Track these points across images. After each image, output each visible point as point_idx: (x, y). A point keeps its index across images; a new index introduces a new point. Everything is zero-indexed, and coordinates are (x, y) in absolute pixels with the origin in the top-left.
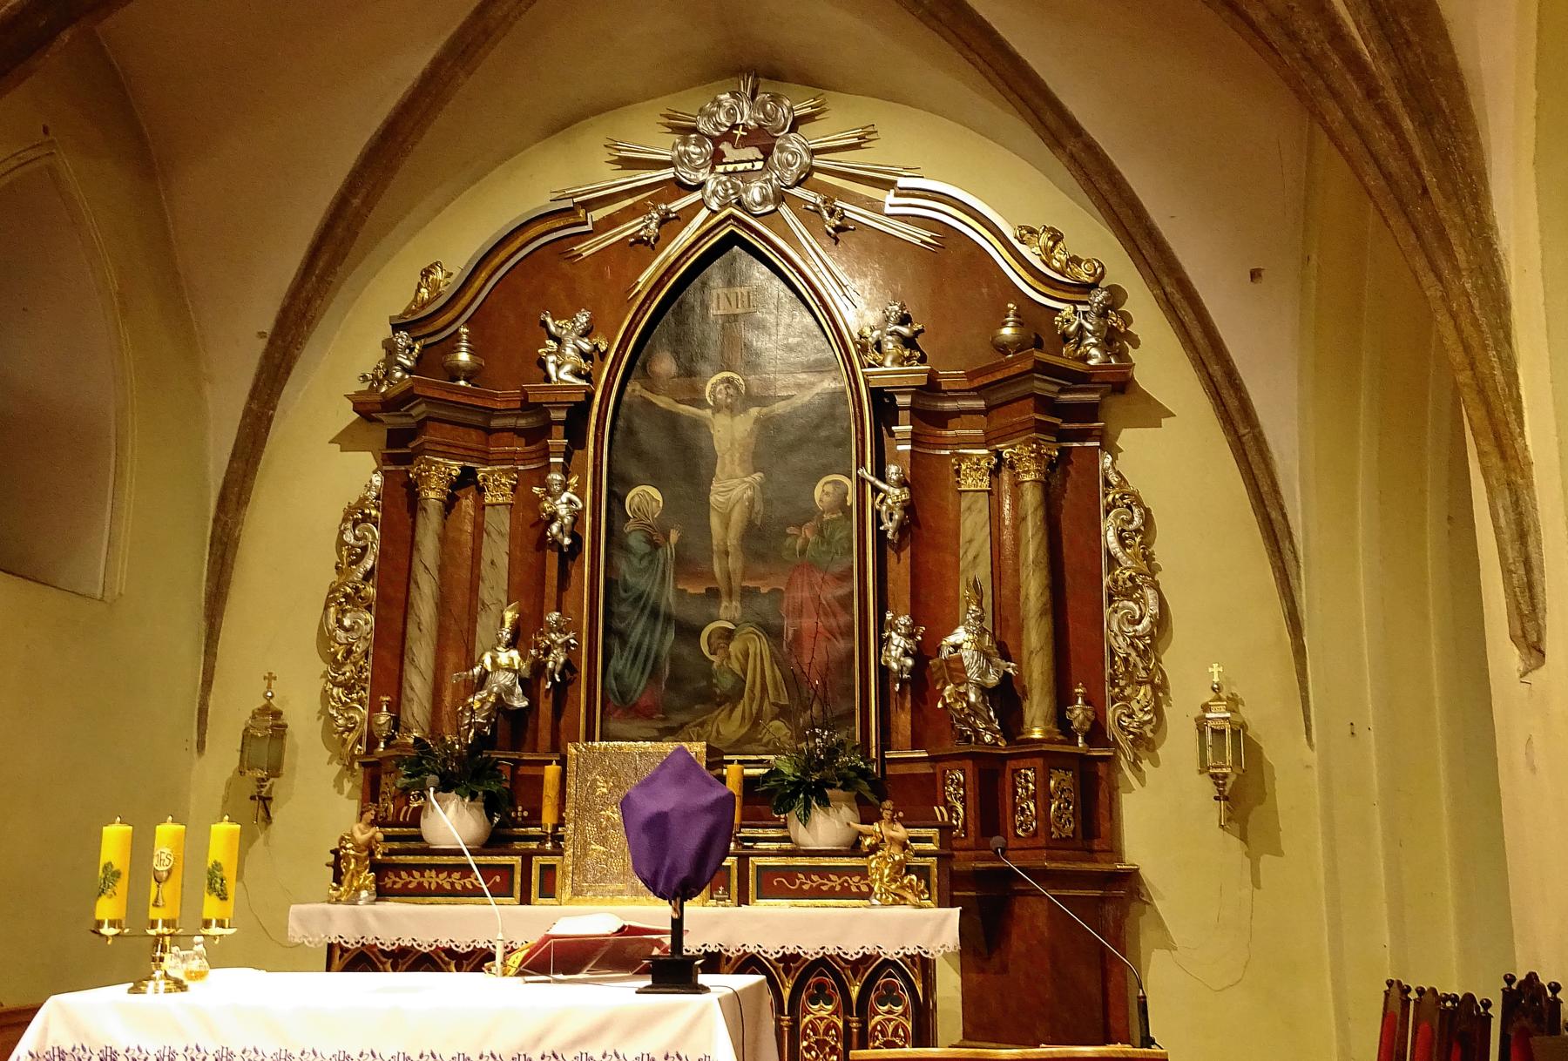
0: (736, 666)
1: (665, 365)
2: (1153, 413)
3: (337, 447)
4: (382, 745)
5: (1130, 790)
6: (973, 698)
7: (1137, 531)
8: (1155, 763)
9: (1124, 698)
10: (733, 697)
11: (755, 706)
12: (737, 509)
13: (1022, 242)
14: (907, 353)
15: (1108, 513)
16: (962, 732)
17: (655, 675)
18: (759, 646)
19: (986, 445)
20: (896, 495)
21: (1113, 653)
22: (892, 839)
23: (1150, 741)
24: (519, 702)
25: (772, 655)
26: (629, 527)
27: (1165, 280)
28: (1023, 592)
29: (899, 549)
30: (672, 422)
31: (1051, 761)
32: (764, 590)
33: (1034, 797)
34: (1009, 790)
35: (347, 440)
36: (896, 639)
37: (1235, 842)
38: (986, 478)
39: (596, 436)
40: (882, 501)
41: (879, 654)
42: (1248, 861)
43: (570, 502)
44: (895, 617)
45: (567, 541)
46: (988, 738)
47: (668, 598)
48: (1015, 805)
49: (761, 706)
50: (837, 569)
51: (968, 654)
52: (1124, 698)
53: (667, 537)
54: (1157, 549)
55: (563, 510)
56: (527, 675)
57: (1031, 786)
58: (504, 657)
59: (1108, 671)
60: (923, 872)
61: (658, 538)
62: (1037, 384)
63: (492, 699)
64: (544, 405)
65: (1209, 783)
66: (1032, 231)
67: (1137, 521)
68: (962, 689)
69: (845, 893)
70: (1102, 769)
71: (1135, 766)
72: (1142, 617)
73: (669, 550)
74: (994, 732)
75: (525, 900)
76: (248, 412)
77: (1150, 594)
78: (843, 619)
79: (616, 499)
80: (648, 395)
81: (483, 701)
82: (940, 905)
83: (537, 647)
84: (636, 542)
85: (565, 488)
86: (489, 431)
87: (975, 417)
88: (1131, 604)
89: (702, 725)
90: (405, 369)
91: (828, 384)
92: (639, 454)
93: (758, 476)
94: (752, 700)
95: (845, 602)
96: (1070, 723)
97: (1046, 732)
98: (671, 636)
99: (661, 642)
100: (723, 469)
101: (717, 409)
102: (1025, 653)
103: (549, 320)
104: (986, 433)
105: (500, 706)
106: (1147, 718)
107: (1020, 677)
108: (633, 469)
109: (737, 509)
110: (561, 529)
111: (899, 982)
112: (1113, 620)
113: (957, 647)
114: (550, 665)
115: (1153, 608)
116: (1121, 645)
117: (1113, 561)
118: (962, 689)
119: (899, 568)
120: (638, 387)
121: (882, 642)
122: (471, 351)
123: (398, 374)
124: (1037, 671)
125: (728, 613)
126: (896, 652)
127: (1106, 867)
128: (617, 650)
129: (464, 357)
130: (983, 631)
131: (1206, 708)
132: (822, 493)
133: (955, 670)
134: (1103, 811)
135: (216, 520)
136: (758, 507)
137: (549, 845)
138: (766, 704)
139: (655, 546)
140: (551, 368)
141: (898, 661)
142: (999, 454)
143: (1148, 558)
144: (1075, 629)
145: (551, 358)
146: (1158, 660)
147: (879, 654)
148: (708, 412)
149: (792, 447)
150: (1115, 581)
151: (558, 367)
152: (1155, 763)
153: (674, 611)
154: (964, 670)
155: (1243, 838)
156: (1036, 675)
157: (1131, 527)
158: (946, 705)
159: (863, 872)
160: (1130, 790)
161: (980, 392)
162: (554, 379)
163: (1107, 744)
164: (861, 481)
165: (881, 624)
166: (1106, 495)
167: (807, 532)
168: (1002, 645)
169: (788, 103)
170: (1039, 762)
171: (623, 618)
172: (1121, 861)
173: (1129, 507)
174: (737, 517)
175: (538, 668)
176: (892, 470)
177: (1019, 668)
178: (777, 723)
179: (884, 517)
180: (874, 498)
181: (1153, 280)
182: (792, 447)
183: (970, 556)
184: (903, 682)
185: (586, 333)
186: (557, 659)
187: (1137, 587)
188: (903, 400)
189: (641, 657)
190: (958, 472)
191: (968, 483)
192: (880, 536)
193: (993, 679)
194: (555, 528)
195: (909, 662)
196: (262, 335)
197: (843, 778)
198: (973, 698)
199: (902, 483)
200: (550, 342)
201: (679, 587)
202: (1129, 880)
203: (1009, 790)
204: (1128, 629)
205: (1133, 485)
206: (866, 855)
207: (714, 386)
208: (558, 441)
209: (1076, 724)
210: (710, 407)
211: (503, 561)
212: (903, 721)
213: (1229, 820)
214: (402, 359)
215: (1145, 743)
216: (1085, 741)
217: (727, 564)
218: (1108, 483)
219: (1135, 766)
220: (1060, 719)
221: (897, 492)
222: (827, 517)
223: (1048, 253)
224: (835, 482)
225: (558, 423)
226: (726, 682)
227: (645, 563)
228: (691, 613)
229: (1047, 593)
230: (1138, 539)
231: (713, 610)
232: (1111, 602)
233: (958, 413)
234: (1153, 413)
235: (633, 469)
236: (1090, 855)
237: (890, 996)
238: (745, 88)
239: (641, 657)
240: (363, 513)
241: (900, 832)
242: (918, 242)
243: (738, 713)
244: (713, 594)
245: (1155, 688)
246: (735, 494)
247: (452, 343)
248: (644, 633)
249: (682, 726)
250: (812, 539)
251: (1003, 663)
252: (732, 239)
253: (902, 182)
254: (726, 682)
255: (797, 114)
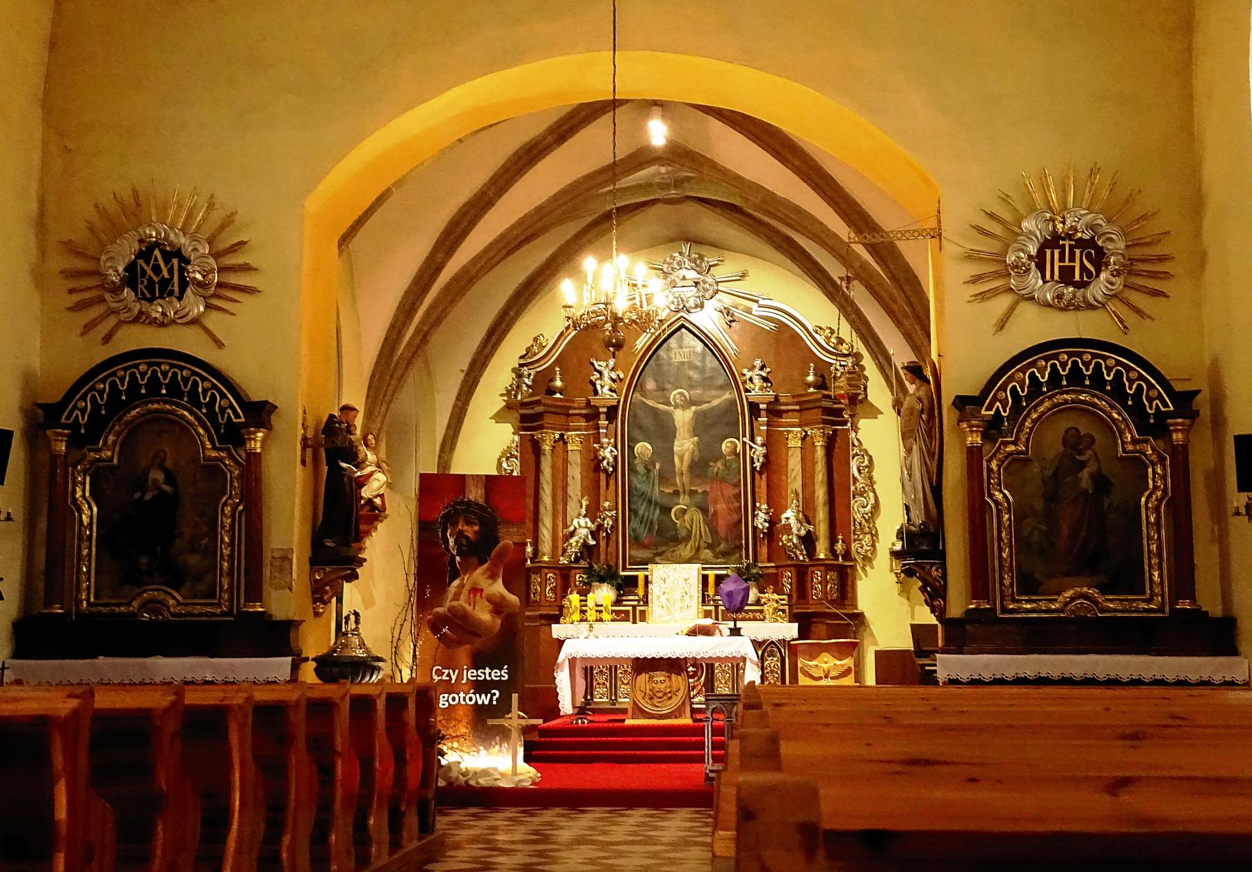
0: (688, 527)
1: (650, 385)
2: (874, 412)
3: (494, 421)
4: (529, 561)
5: (861, 579)
6: (795, 541)
7: (866, 467)
8: (872, 568)
9: (860, 540)
10: (687, 538)
11: (697, 544)
12: (687, 454)
13: (817, 333)
14: (765, 385)
15: (853, 458)
16: (789, 555)
17: (651, 529)
18: (698, 516)
19: (800, 426)
20: (760, 451)
21: (854, 520)
22: (773, 599)
23: (870, 558)
24: (592, 542)
25: (704, 520)
26: (636, 462)
27: (880, 356)
28: (816, 495)
29: (760, 473)
30: (655, 412)
31: (829, 568)
32: (700, 491)
33: (820, 583)
34: (809, 579)
35: (499, 417)
36: (761, 514)
37: (905, 601)
38: (800, 441)
39: (622, 419)
40: (754, 453)
41: (753, 521)
42: (910, 609)
43: (612, 451)
44: (761, 505)
45: (611, 469)
46: (801, 558)
47: (656, 494)
48: (812, 586)
49: (699, 543)
50: (734, 481)
51: (793, 521)
52: (860, 540)
53: (655, 467)
54: (874, 474)
55: (608, 455)
56: (594, 529)
57: (820, 578)
58: (583, 521)
59: (853, 528)
60: (783, 611)
61: (651, 467)
62: (823, 402)
63: (582, 541)
64: (927, 668)
65: (894, 576)
66: (821, 328)
67: (866, 463)
68: (790, 537)
69: (755, 619)
70: (849, 571)
71: (863, 569)
72: (867, 504)
73: (656, 472)
74: (803, 556)
75: (634, 622)
76: (455, 406)
77: (871, 494)
78: (736, 504)
79: (631, 449)
80: (644, 400)
81: (577, 542)
82: (790, 622)
83: (600, 518)
84: (640, 469)
85: (609, 444)
86: (569, 415)
87: (795, 413)
88: (863, 499)
89: (673, 551)
90: (527, 385)
91: (727, 396)
92: (640, 427)
93: (696, 438)
94: (695, 541)
95: (737, 497)
96: (836, 551)
97: (826, 555)
98: (658, 511)
99: (653, 515)
100: (679, 435)
101: (676, 407)
102: (817, 521)
103: (595, 362)
104: (800, 421)
105: (585, 545)
106: (869, 548)
107: (815, 533)
108: (636, 434)
109: (687, 454)
110: (608, 463)
111: (766, 654)
112: (855, 504)
113: (787, 519)
114: (606, 525)
115: (872, 501)
116: (858, 517)
117: (855, 479)
118: (790, 537)
119: (762, 483)
120: (638, 395)
121: (754, 516)
122: (562, 380)
123: (525, 388)
124: (822, 529)
125: (683, 502)
126: (761, 520)
127: (851, 612)
128: (633, 517)
129: (558, 383)
130: (799, 511)
131: (893, 544)
132: (725, 446)
133: (787, 529)
134: (849, 589)
135: (439, 457)
136: (696, 453)
137: (642, 603)
138: (702, 542)
139: (649, 471)
140: (598, 387)
141: (761, 524)
142: (806, 432)
143: (871, 478)
144: (839, 510)
145: (598, 382)
146: (874, 522)
147: (753, 521)
148: (672, 408)
149: (713, 425)
150: (856, 489)
151: (602, 387)
152: (872, 568)
153: (659, 500)
154: (791, 529)
155: (908, 599)
156: (822, 530)
157: (864, 465)
158: (783, 544)
159: (761, 611)
160: (861, 579)
161: (797, 403)
162: (600, 392)
163: (852, 560)
164: (744, 443)
165: (754, 508)
166: (853, 450)
167: (719, 464)
168: (807, 517)
169: (706, 259)
170: (822, 568)
171: (635, 503)
172: (856, 609)
173: (863, 456)
174: (687, 458)
175: (600, 527)
176: (759, 440)
177: (814, 528)
178: (707, 551)
179: (755, 460)
180: (750, 451)
181: (875, 357)
182: (713, 425)
183: (793, 477)
184: (764, 533)
185: (612, 369)
186: (608, 523)
187: (865, 491)
188: (762, 406)
189: (644, 522)
190: (787, 439)
191: (791, 443)
192: (753, 469)
193: (803, 532)
194: (605, 463)
195: (767, 525)
196: (462, 371)
197: (754, 577)
198: (795, 541)
199: (763, 445)
200: (595, 373)
201: (662, 489)
202: (859, 618)
203: (809, 579)
204: (861, 509)
205: (865, 446)
206: (763, 605)
207: (675, 396)
208: (603, 422)
209: (839, 551)
210: (672, 405)
211: (578, 476)
212: (764, 551)
213: (902, 592)
214: (526, 380)
215: (867, 559)
216: (842, 558)
217: (682, 479)
218: (853, 445)
219: (863, 569)
220: (832, 551)
221: (761, 448)
222: (728, 458)
223: (828, 339)
224: (731, 442)
225: (603, 413)
226: (683, 533)
227: (645, 478)
228: (665, 501)
229: (826, 496)
230: (866, 470)
231: (676, 500)
232: (854, 498)
233: (788, 411)
234: (874, 412)
235: (636, 434)
236: (843, 606)
237: (772, 654)
238: (685, 249)
239: (644, 522)
240: (511, 453)
241: (776, 597)
242: (768, 329)
243: (689, 547)
244: (676, 493)
245: (872, 535)
246: (686, 447)
247: (553, 379)
248: (645, 510)
249: (664, 552)
250: (721, 467)
251: (808, 526)
252: (683, 326)
253: (762, 302)
254: (683, 533)
255: (711, 264)
